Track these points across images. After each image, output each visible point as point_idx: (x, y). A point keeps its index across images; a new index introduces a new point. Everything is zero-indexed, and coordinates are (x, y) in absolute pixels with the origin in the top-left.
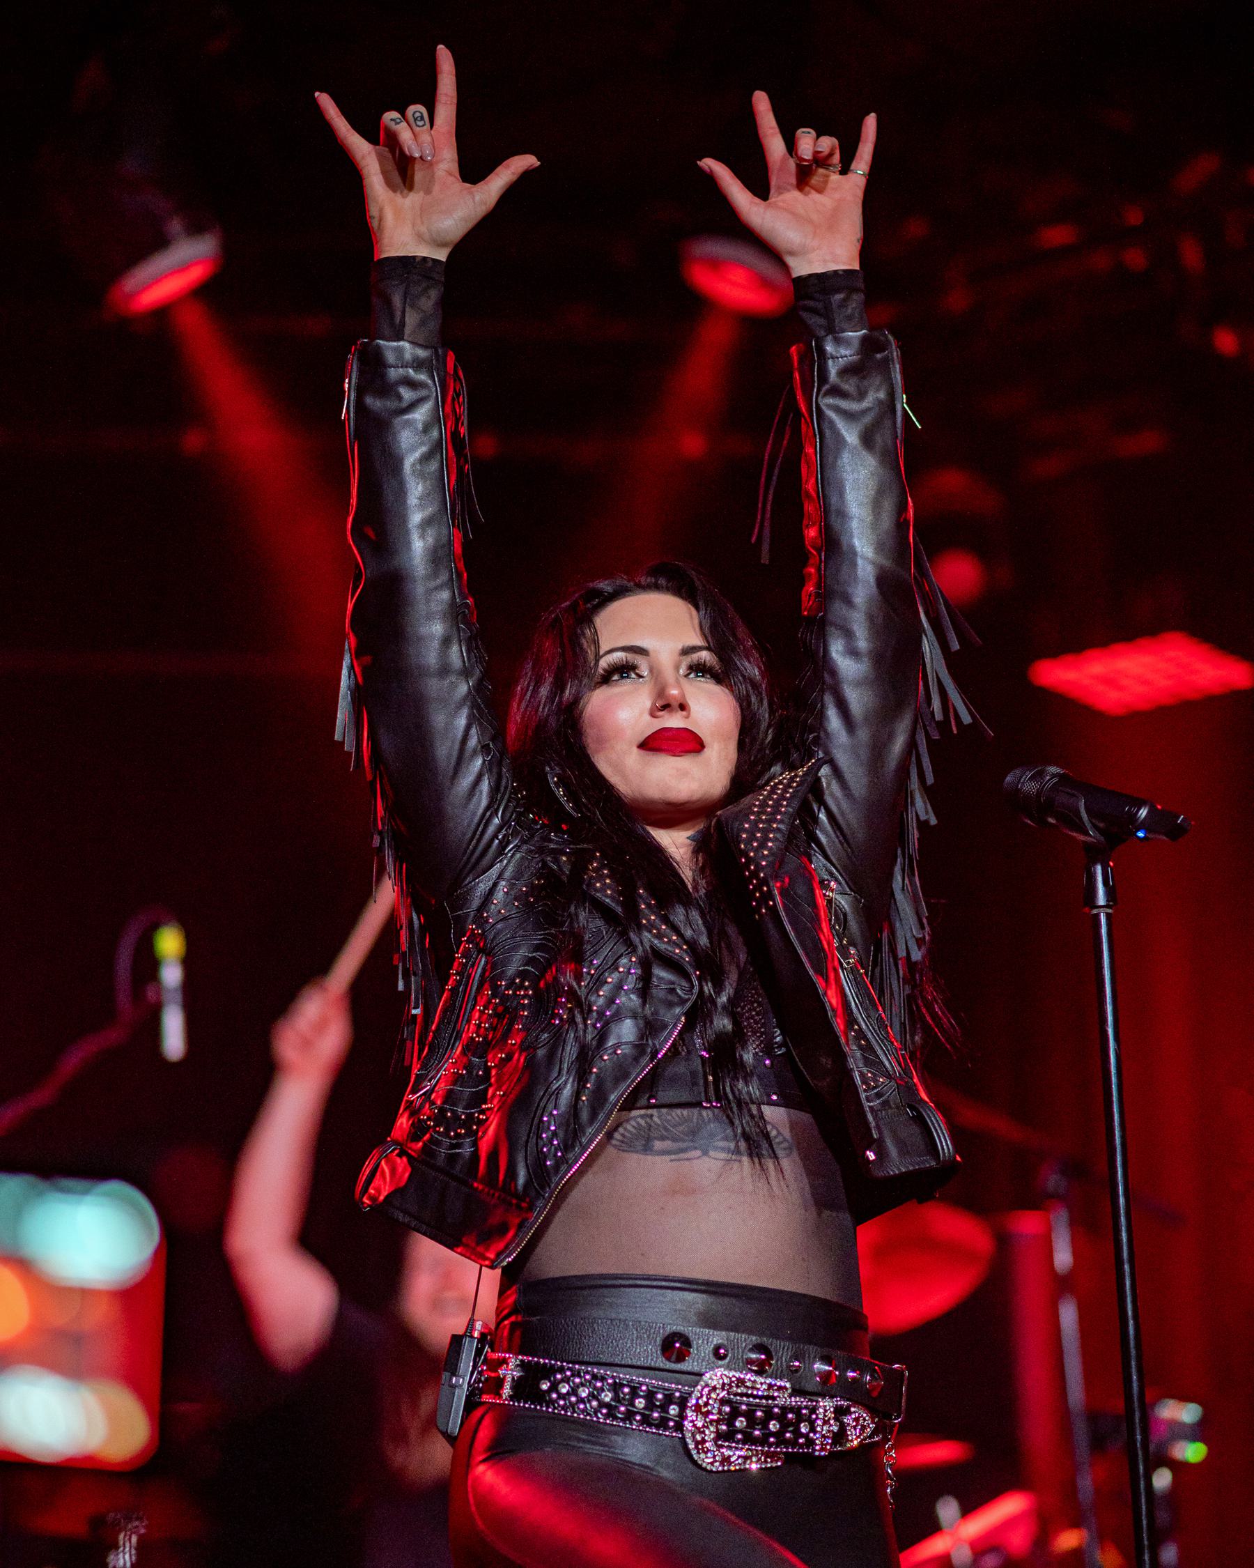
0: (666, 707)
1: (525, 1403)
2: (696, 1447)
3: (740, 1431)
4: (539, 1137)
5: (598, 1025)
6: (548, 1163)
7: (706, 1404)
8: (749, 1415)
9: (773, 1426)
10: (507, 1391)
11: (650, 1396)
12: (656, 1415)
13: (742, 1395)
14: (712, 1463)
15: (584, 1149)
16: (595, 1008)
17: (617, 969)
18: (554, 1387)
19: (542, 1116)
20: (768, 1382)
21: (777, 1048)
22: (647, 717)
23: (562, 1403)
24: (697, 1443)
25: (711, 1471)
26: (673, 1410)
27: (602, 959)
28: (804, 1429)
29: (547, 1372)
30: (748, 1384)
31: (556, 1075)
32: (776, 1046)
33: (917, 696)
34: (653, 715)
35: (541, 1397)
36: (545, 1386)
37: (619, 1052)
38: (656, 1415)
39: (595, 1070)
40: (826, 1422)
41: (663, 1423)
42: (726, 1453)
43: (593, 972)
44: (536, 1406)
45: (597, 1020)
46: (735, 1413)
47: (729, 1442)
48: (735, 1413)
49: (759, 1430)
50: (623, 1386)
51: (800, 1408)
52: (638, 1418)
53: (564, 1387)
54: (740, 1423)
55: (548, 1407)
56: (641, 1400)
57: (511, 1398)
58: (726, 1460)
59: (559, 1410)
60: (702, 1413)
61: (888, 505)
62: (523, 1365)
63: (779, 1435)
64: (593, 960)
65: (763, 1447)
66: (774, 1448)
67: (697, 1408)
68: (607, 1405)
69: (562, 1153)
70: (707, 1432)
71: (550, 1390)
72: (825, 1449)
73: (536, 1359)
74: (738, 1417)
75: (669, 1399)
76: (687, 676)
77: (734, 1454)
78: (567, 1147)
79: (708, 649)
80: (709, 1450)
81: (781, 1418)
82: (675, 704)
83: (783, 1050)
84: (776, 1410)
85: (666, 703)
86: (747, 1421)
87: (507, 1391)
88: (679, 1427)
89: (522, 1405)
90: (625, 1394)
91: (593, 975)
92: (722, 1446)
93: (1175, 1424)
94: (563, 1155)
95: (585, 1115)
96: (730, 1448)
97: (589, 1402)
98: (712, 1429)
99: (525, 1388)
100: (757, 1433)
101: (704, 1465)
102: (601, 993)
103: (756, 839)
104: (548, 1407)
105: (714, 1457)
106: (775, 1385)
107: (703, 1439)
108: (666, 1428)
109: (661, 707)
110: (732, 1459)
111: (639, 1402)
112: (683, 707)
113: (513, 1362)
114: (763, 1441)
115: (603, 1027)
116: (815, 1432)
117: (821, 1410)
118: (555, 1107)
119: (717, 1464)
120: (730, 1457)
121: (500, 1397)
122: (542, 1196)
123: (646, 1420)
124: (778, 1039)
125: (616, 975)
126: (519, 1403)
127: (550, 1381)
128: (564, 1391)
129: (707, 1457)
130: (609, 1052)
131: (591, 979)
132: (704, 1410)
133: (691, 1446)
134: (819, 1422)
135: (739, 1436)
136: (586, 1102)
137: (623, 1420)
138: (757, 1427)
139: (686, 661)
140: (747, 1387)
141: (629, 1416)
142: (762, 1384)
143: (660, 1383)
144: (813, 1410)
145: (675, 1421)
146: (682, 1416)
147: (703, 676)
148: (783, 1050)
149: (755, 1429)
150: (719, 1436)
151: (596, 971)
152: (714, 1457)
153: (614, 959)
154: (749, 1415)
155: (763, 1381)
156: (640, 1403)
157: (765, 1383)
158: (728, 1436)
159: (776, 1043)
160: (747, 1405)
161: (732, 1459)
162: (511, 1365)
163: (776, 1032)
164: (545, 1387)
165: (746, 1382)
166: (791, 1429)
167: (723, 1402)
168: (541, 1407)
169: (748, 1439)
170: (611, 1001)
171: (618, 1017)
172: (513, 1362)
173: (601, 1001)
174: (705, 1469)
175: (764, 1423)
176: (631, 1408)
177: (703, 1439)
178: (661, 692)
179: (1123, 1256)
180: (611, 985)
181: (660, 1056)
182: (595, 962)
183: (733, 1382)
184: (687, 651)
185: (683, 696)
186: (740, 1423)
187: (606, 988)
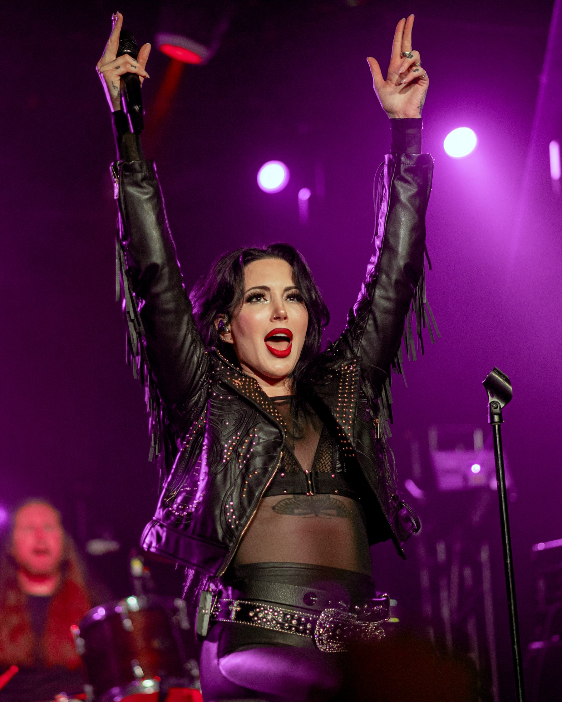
0: (278, 318)
1: (242, 622)
2: (319, 642)
3: (308, 629)
4: (226, 514)
10: (233, 616)
11: (299, 620)
12: (301, 628)
15: (248, 518)
16: (242, 454)
17: (249, 435)
18: (256, 615)
19: (226, 505)
21: (337, 469)
22: (268, 321)
23: (259, 621)
24: (319, 640)
27: (241, 431)
29: (253, 608)
31: (229, 486)
32: (337, 468)
33: (386, 198)
34: (271, 321)
35: (250, 619)
36: (251, 614)
37: (256, 473)
38: (301, 628)
39: (247, 482)
41: (304, 631)
43: (238, 438)
50: (287, 614)
52: (293, 629)
53: (260, 615)
55: (253, 623)
56: (295, 621)
57: (235, 619)
62: (240, 605)
71: (254, 616)
73: (247, 602)
75: (307, 620)
76: (286, 300)
78: (240, 518)
79: (296, 288)
82: (282, 317)
83: (340, 470)
85: (277, 316)
87: (233, 616)
89: (240, 622)
90: (288, 618)
91: (238, 440)
92: (330, 642)
94: (239, 522)
95: (246, 503)
97: (272, 621)
99: (242, 615)
102: (244, 447)
104: (253, 623)
108: (306, 634)
109: (276, 317)
112: (285, 318)
113: (236, 603)
118: (232, 501)
121: (230, 619)
123: (297, 630)
124: (338, 466)
125: (249, 438)
126: (239, 621)
127: (254, 612)
128: (261, 616)
130: (252, 473)
132: (323, 626)
137: (287, 630)
139: (285, 295)
141: (290, 628)
146: (313, 628)
147: (292, 300)
148: (340, 470)
150: (329, 637)
151: (239, 438)
156: (294, 622)
159: (337, 467)
162: (235, 605)
163: (338, 462)
164: (251, 614)
168: (250, 623)
170: (248, 450)
171: (253, 456)
172: (236, 603)
173: (244, 451)
176: (291, 625)
177: (322, 638)
178: (276, 311)
179: (128, 280)
182: (239, 434)
184: (287, 289)
185: (286, 313)
187: (246, 445)
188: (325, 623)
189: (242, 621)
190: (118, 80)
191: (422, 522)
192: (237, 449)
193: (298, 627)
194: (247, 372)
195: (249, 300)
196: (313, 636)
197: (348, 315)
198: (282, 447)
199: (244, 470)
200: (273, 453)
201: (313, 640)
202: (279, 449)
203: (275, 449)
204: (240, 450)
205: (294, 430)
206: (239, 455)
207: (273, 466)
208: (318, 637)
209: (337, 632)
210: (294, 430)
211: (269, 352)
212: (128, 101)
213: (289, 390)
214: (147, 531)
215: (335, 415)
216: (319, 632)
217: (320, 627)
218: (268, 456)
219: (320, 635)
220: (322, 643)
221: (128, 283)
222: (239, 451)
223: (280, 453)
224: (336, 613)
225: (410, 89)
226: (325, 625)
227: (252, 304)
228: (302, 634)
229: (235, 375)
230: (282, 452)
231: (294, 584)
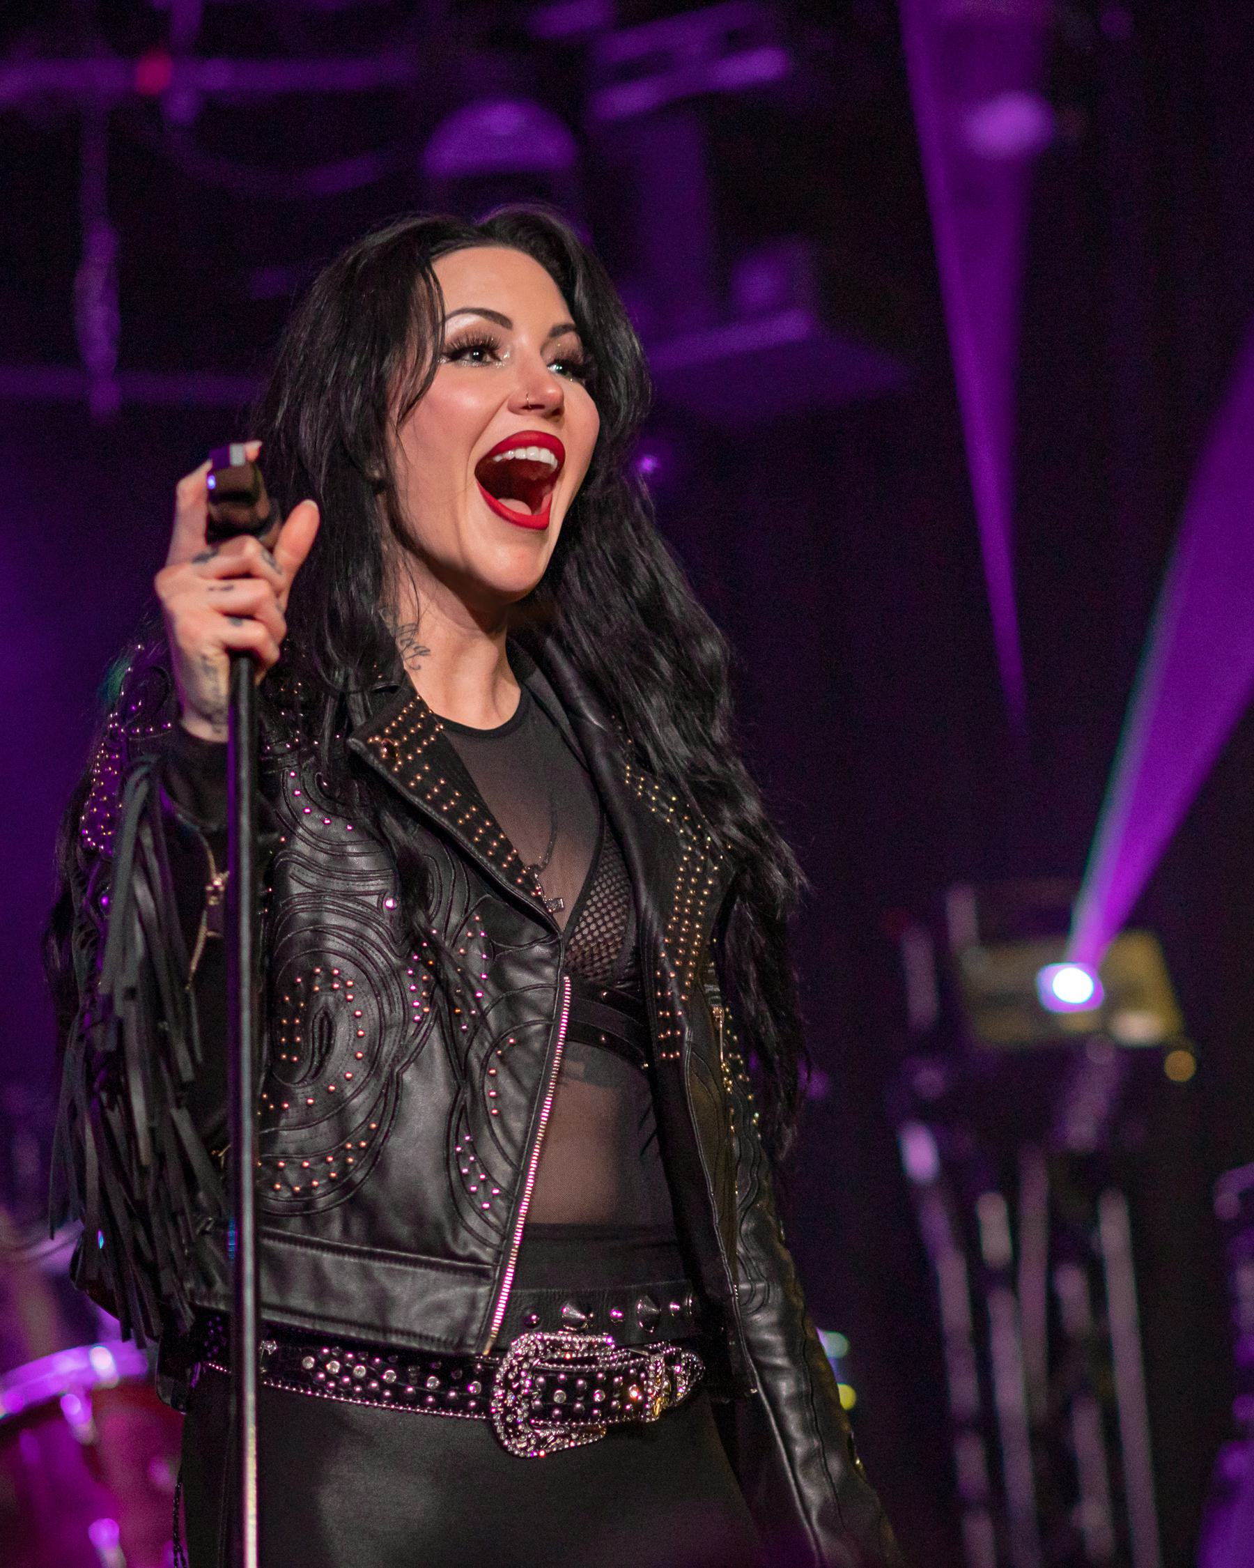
2: (506, 1432)
3: (473, 1397)
7: (518, 1378)
18: (320, 1366)
20: (588, 1340)
24: (507, 1425)
30: (567, 1347)
35: (306, 1378)
36: (310, 1363)
41: (461, 1405)
42: (541, 1434)
44: (298, 1389)
46: (552, 1384)
47: (544, 1420)
58: (542, 1442)
59: (328, 1395)
60: (513, 1390)
63: (604, 1405)
65: (586, 1421)
66: (429, 1410)
67: (507, 1384)
68: (391, 1387)
70: (519, 1412)
71: (315, 1370)
74: (555, 1391)
77: (551, 1434)
80: (522, 1433)
84: (600, 1375)
86: (397, 1374)
88: (484, 1407)
93: (944, 925)
96: (544, 1427)
98: (525, 1406)
100: (410, 1389)
103: (697, 875)
105: (529, 1440)
106: (597, 1342)
107: (515, 1420)
108: (467, 1410)
111: (359, 1370)
117: (652, 1368)
119: (531, 1448)
120: (546, 1438)
123: (442, 1403)
129: (519, 1443)
133: (500, 1430)
135: (557, 1412)
136: (302, 985)
138: (579, 1399)
140: (566, 1351)
142: (581, 1344)
143: (555, 1366)
144: (642, 1368)
146: (487, 1395)
150: (533, 1413)
152: (529, 1440)
154: (569, 1387)
155: (582, 1340)
157: (585, 1342)
158: (544, 1413)
160: (565, 1373)
165: (563, 1345)
166: (617, 1396)
177: (515, 1420)
183: (548, 1347)
186: (559, 1396)
188: (518, 1378)
189: (284, 1384)
190: (213, 645)
193: (443, 1393)
194: (451, 1185)
195: (456, 355)
196: (489, 1414)
201: (490, 1423)
208: (503, 1417)
209: (556, 1399)
215: (661, 938)
216: (504, 1406)
217: (507, 1392)
219: (508, 1411)
220: (514, 1433)
221: (473, 782)
224: (546, 1347)
225: (387, 577)
226: (522, 1382)
227: (482, 366)
228: (455, 1411)
229: (272, 1110)
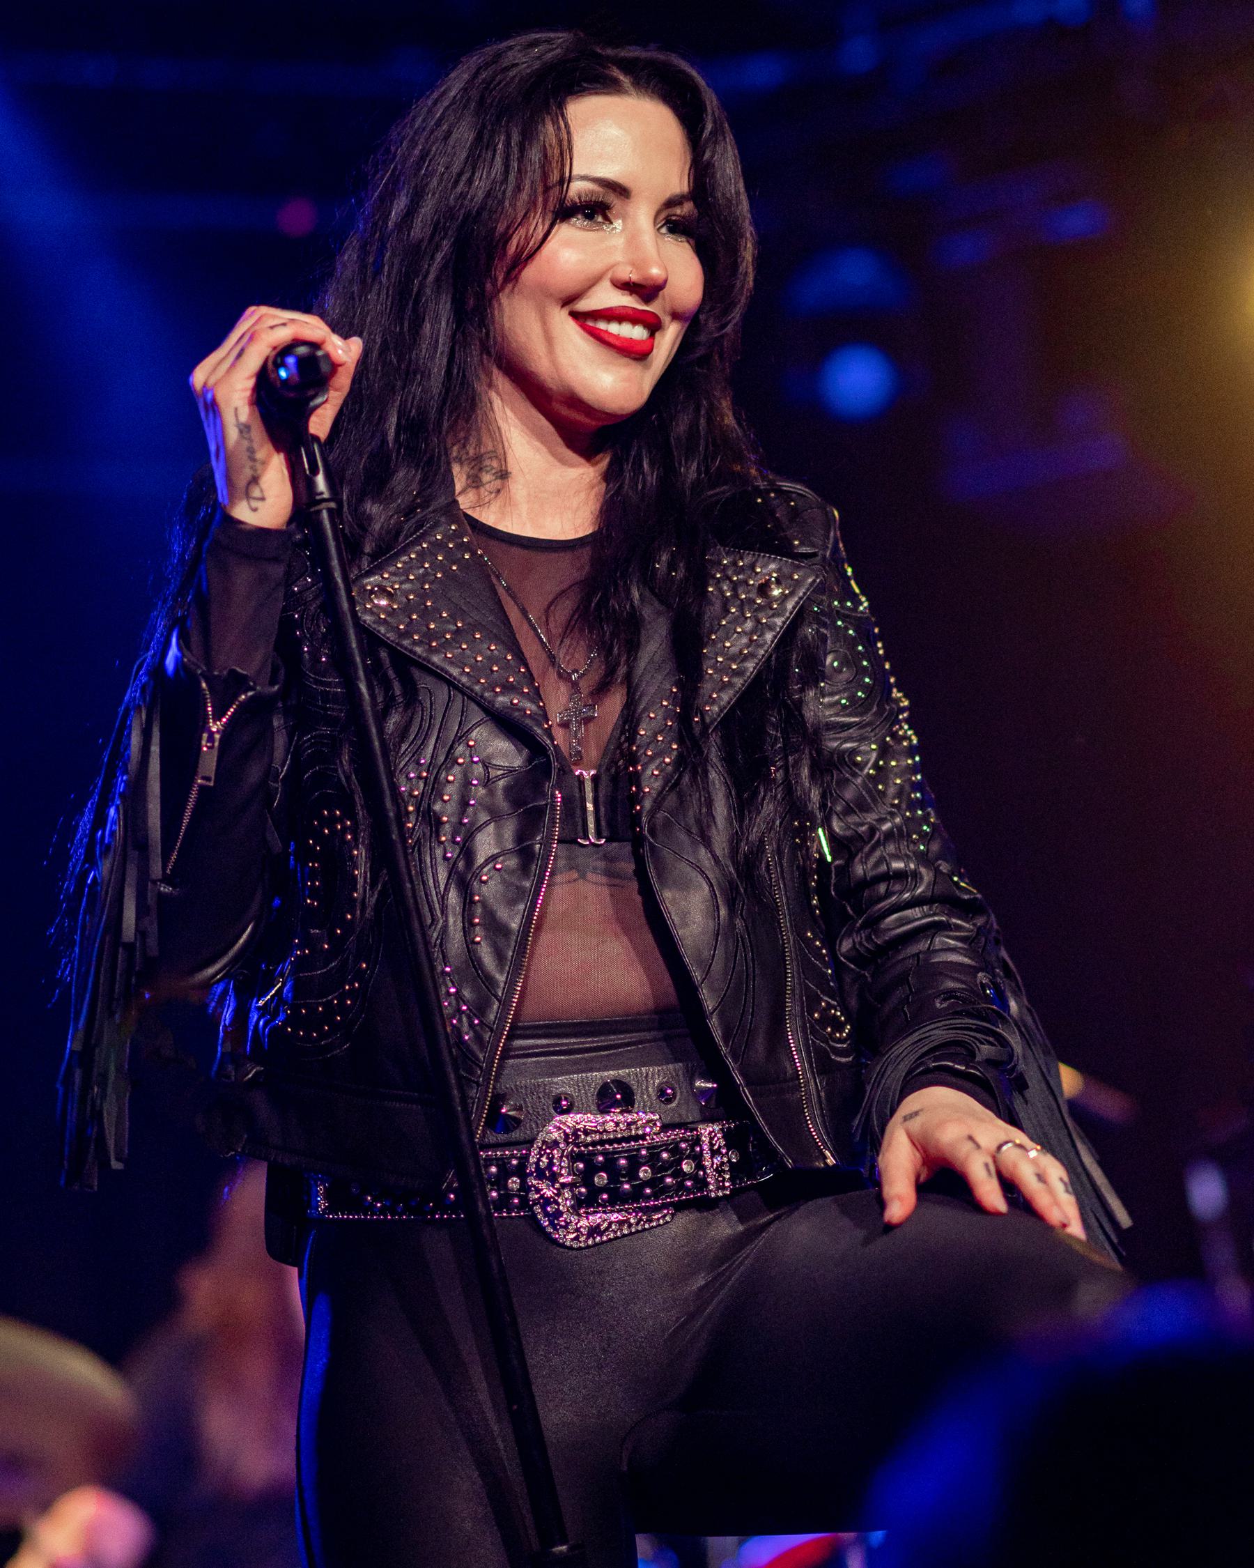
2: (552, 1224)
5: (458, 839)
6: (467, 1038)
8: (610, 1165)
9: (644, 1173)
13: (594, 1144)
14: (576, 1238)
25: (580, 1248)
26: (514, 1183)
28: (686, 1167)
40: (714, 1153)
43: (425, 774)
45: (455, 834)
46: (591, 1170)
48: (591, 1170)
49: (627, 1182)
51: (677, 1144)
54: (601, 1179)
61: (683, 158)
64: (419, 759)
67: (540, 1174)
69: (478, 1018)
72: (724, 1188)
81: (653, 1158)
91: (426, 778)
101: (568, 1243)
110: (602, 1228)
114: (636, 1194)
115: (465, 841)
116: (703, 1168)
118: (446, 962)
122: (474, 1082)
125: (456, 769)
131: (425, 784)
134: (707, 1156)
144: (697, 1141)
145: (519, 1197)
149: (622, 1183)
151: (428, 772)
153: (447, 749)
160: (602, 1154)
161: (602, 1228)
167: (574, 1158)
169: (617, 1198)
173: (451, 808)
174: (571, 1248)
175: (632, 1173)
180: (456, 785)
181: (234, 707)
186: (601, 1179)
187: (449, 789)
191: (693, 65)
192: (429, 805)
197: (843, 1018)
198: (554, 777)
199: (461, 865)
200: (534, 800)
202: (548, 786)
203: (538, 790)
204: (437, 807)
205: (464, 699)
206: (440, 823)
207: (542, 838)
210: (464, 699)
211: (592, 339)
212: (1124, 1219)
213: (484, 431)
214: (454, 923)
218: (519, 815)
222: (435, 812)
223: (553, 796)
230: (557, 792)
231: (654, 996)
